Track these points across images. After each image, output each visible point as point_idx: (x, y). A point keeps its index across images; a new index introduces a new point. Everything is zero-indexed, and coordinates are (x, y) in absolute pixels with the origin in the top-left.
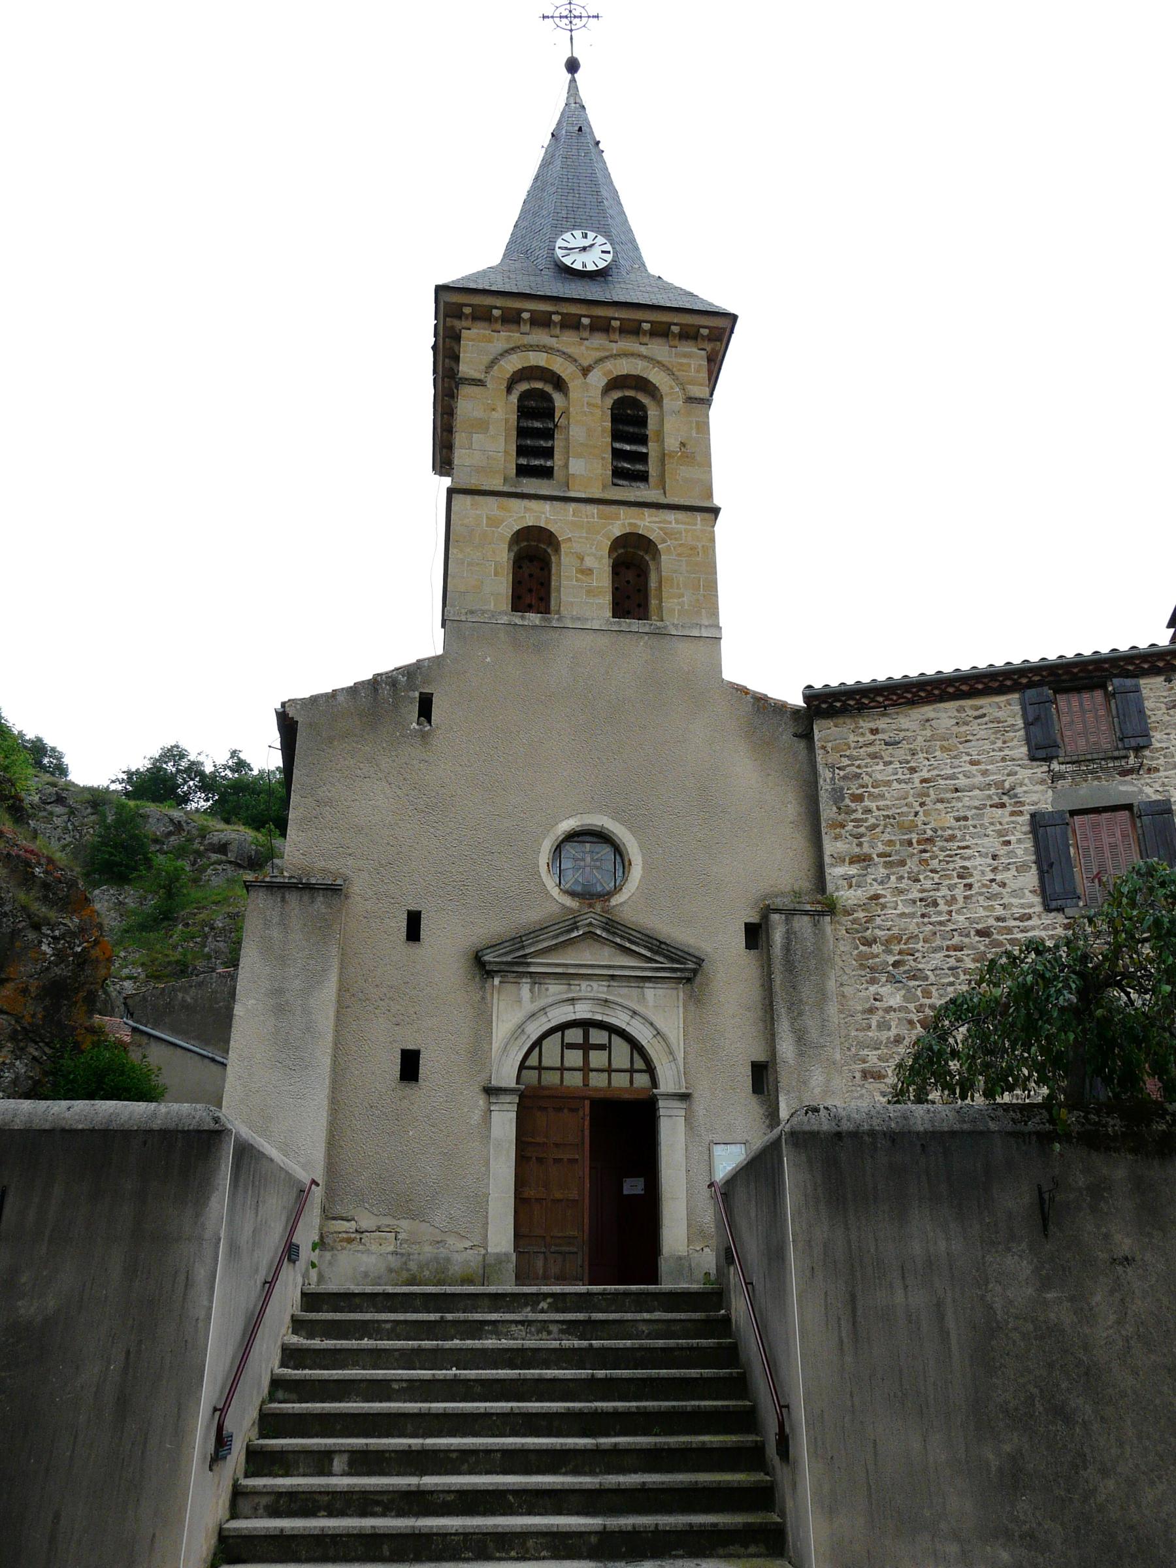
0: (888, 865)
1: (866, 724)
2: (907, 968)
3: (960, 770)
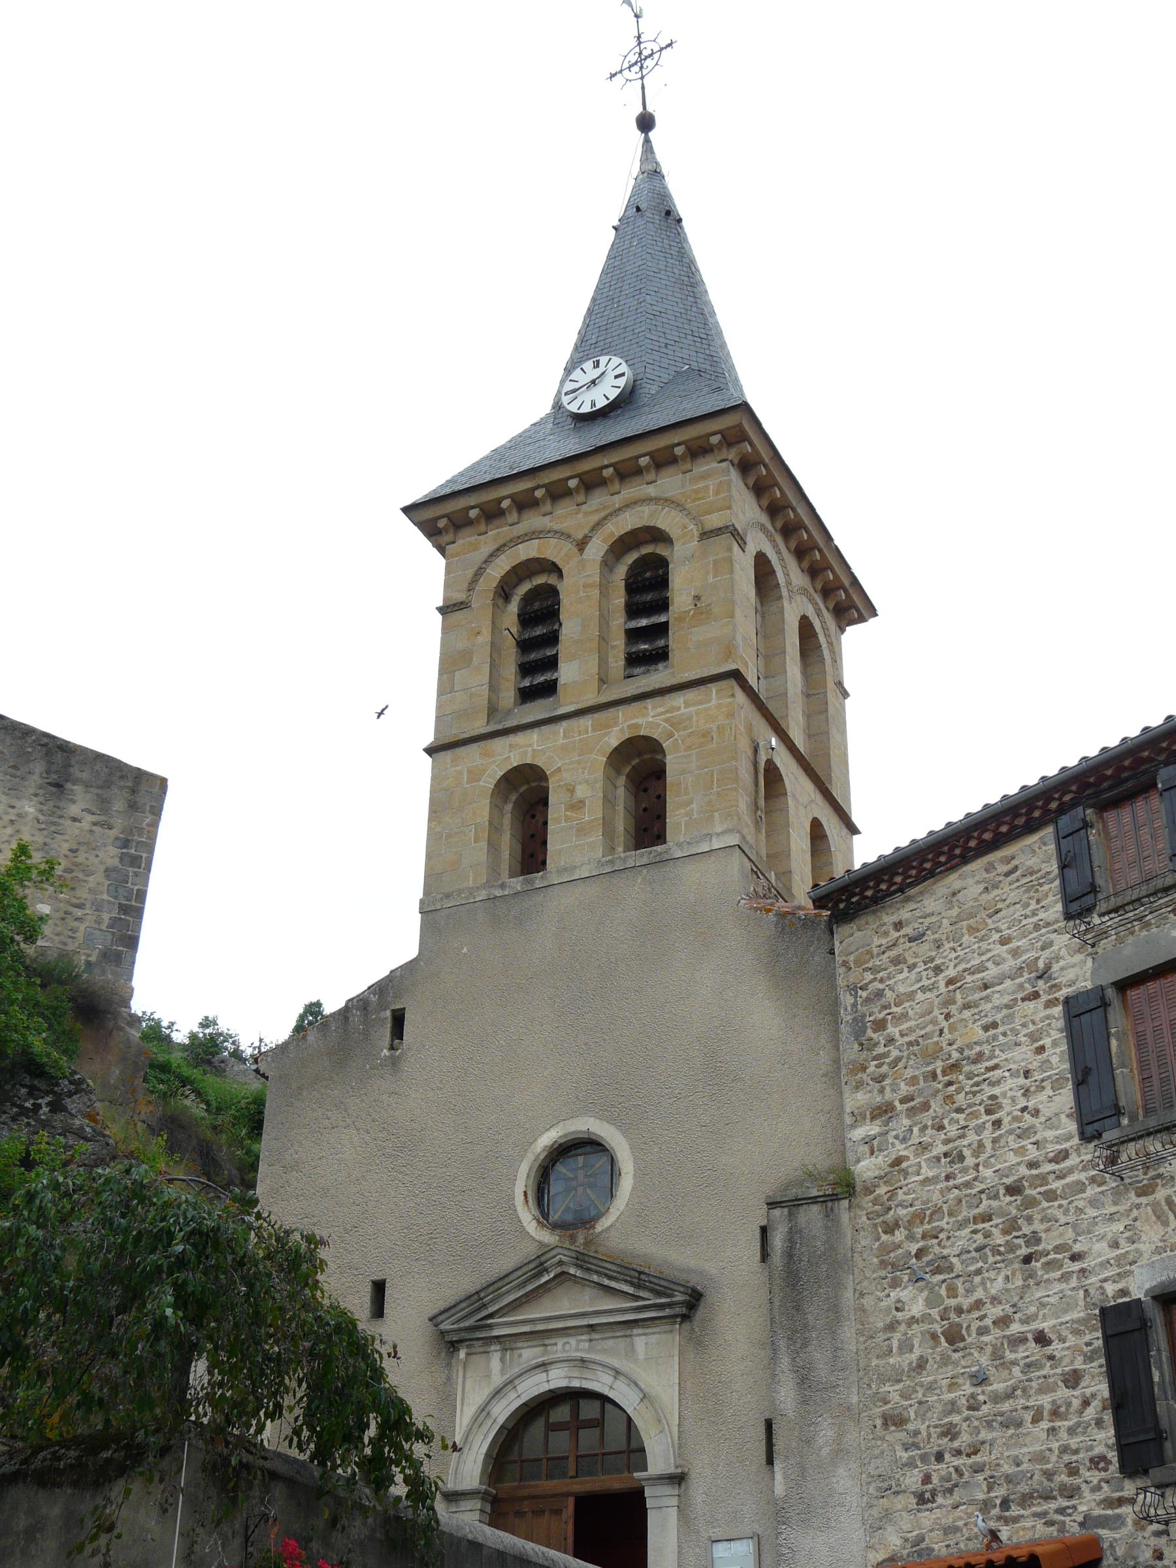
0: (912, 1112)
1: (889, 919)
2: (930, 1257)
3: (989, 955)
